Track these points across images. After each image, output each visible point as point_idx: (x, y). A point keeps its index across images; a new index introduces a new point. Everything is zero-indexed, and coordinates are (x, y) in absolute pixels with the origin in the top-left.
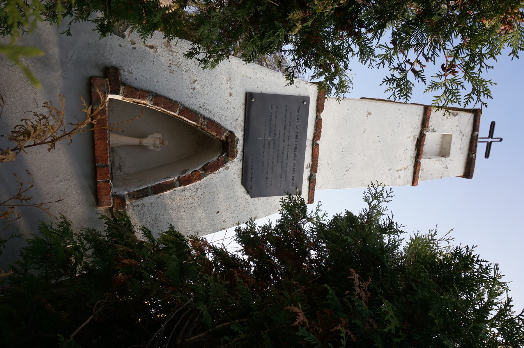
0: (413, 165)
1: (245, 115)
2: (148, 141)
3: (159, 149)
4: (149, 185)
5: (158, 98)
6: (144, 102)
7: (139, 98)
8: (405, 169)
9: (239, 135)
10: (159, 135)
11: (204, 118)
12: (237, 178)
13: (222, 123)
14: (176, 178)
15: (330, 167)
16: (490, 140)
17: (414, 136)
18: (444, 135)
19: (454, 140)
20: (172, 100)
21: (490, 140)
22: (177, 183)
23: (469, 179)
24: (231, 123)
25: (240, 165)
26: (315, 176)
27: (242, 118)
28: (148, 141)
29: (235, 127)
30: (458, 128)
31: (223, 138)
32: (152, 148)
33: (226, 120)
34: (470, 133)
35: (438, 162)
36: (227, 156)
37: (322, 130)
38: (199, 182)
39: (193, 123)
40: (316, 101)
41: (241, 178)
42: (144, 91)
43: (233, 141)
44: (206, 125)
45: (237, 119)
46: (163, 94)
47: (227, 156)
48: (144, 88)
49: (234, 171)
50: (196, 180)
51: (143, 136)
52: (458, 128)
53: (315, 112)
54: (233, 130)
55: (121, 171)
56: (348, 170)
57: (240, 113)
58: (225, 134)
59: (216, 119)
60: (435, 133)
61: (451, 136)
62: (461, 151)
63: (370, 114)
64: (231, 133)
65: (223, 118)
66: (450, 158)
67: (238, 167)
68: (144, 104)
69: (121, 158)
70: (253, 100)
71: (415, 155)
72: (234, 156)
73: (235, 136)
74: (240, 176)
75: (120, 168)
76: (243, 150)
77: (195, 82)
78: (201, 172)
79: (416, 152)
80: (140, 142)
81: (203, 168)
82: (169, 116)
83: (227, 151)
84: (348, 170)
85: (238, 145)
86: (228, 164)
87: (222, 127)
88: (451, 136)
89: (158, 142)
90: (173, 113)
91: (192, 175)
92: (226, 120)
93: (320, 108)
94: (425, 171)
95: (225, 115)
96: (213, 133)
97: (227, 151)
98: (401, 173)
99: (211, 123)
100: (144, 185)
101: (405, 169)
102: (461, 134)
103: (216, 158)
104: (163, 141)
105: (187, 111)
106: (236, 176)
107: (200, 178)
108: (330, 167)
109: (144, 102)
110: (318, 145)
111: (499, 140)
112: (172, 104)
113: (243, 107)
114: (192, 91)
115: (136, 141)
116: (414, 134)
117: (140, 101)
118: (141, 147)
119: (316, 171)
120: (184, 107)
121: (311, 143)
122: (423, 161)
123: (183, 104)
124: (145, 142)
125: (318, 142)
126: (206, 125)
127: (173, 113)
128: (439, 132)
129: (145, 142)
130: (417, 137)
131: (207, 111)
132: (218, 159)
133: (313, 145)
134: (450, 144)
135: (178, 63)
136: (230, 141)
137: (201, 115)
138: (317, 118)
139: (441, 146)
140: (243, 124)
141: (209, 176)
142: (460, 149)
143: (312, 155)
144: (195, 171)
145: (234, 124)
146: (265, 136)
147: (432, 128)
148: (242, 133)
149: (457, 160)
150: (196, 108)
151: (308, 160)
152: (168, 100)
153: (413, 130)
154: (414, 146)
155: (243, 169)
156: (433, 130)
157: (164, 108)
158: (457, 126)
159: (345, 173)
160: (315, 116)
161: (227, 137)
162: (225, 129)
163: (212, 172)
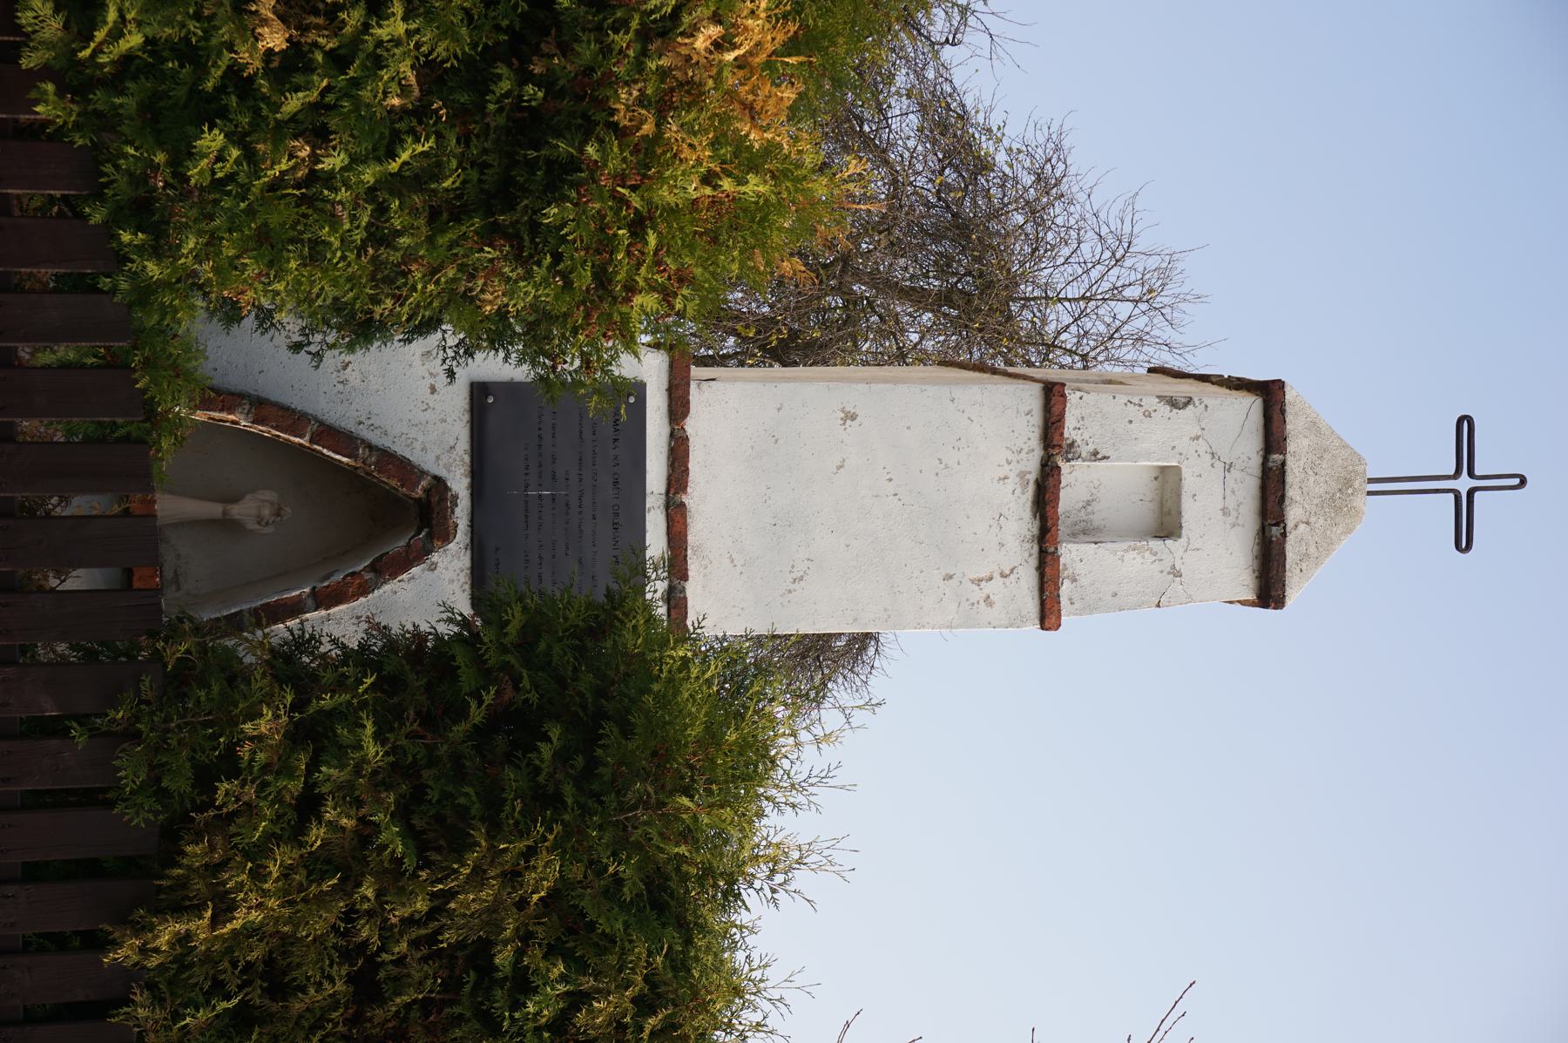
0: (1034, 562)
1: (472, 436)
2: (243, 511)
3: (269, 530)
4: (245, 607)
5: (262, 407)
6: (231, 417)
7: (221, 410)
8: (1003, 576)
9: (460, 484)
10: (270, 496)
11: (370, 447)
12: (458, 591)
13: (416, 457)
14: (307, 590)
15: (739, 569)
16: (1464, 484)
17: (1022, 475)
18: (1163, 469)
19: (1189, 483)
20: (294, 411)
21: (1464, 484)
22: (310, 602)
23: (1269, 611)
24: (438, 458)
25: (465, 561)
26: (683, 590)
27: (464, 445)
28: (243, 511)
29: (448, 467)
30: (1202, 446)
31: (419, 492)
32: (251, 525)
33: (424, 449)
34: (1256, 460)
35: (1132, 554)
36: (430, 536)
37: (690, 466)
38: (362, 599)
39: (345, 460)
40: (665, 394)
41: (468, 591)
42: (233, 394)
43: (443, 499)
44: (376, 464)
45: (452, 448)
46: (275, 396)
47: (430, 536)
48: (232, 388)
49: (449, 575)
50: (355, 597)
51: (235, 499)
52: (1202, 446)
53: (666, 420)
54: (442, 473)
55: (178, 589)
56: (801, 579)
57: (460, 432)
58: (423, 483)
59: (400, 449)
60: (1103, 463)
61: (1177, 470)
62: (1231, 519)
63: (853, 417)
64: (439, 483)
65: (418, 446)
66: (1183, 541)
67: (460, 565)
68: (233, 422)
69: (179, 556)
70: (491, 400)
71: (1036, 531)
72: (446, 536)
73: (447, 489)
74: (467, 587)
75: (176, 581)
76: (472, 521)
77: (345, 368)
78: (368, 576)
79: (1037, 523)
80: (225, 513)
81: (373, 568)
82: (288, 445)
83: (429, 526)
84: (801, 579)
85: (458, 511)
86: (435, 557)
87: (413, 467)
88: (1177, 470)
89: (266, 512)
90: (297, 440)
91: (344, 584)
92: (424, 449)
93: (678, 408)
94: (1084, 581)
95: (421, 438)
96: (394, 483)
97: (429, 526)
98: (995, 588)
99: (388, 458)
100: (235, 605)
101: (1003, 576)
102: (1220, 466)
103: (402, 543)
104: (280, 509)
105: (330, 434)
106: (456, 586)
107: (364, 590)
108: (739, 569)
109: (231, 417)
110: (683, 505)
111: (1516, 481)
112: (293, 419)
113: (466, 417)
114: (340, 387)
115: (214, 510)
116: (1021, 467)
117: (223, 415)
118: (227, 525)
119: (685, 577)
120: (322, 423)
121: (661, 501)
122: (1070, 554)
123: (320, 417)
124: (236, 510)
125: (685, 499)
126: (376, 464)
127: (297, 440)
128: (1119, 459)
129: (236, 510)
130: (1032, 477)
131: (378, 432)
132: (408, 545)
133: (667, 507)
134: (1179, 496)
135: (162, 765)
136: (435, 499)
137: (363, 441)
138: (672, 435)
139: (1162, 505)
140: (467, 459)
141: (386, 588)
142: (1225, 511)
143: (669, 533)
144: (353, 574)
145: (444, 459)
146: (527, 487)
147: (1091, 448)
148: (466, 481)
149: (1219, 543)
150: (350, 425)
151: (656, 543)
152: (286, 410)
153: (1014, 458)
154: (1029, 504)
155: (473, 569)
156: (1095, 453)
157: (276, 428)
158: (1197, 438)
159: (792, 587)
160: (666, 430)
161: (427, 491)
162: (423, 473)
163: (394, 576)
